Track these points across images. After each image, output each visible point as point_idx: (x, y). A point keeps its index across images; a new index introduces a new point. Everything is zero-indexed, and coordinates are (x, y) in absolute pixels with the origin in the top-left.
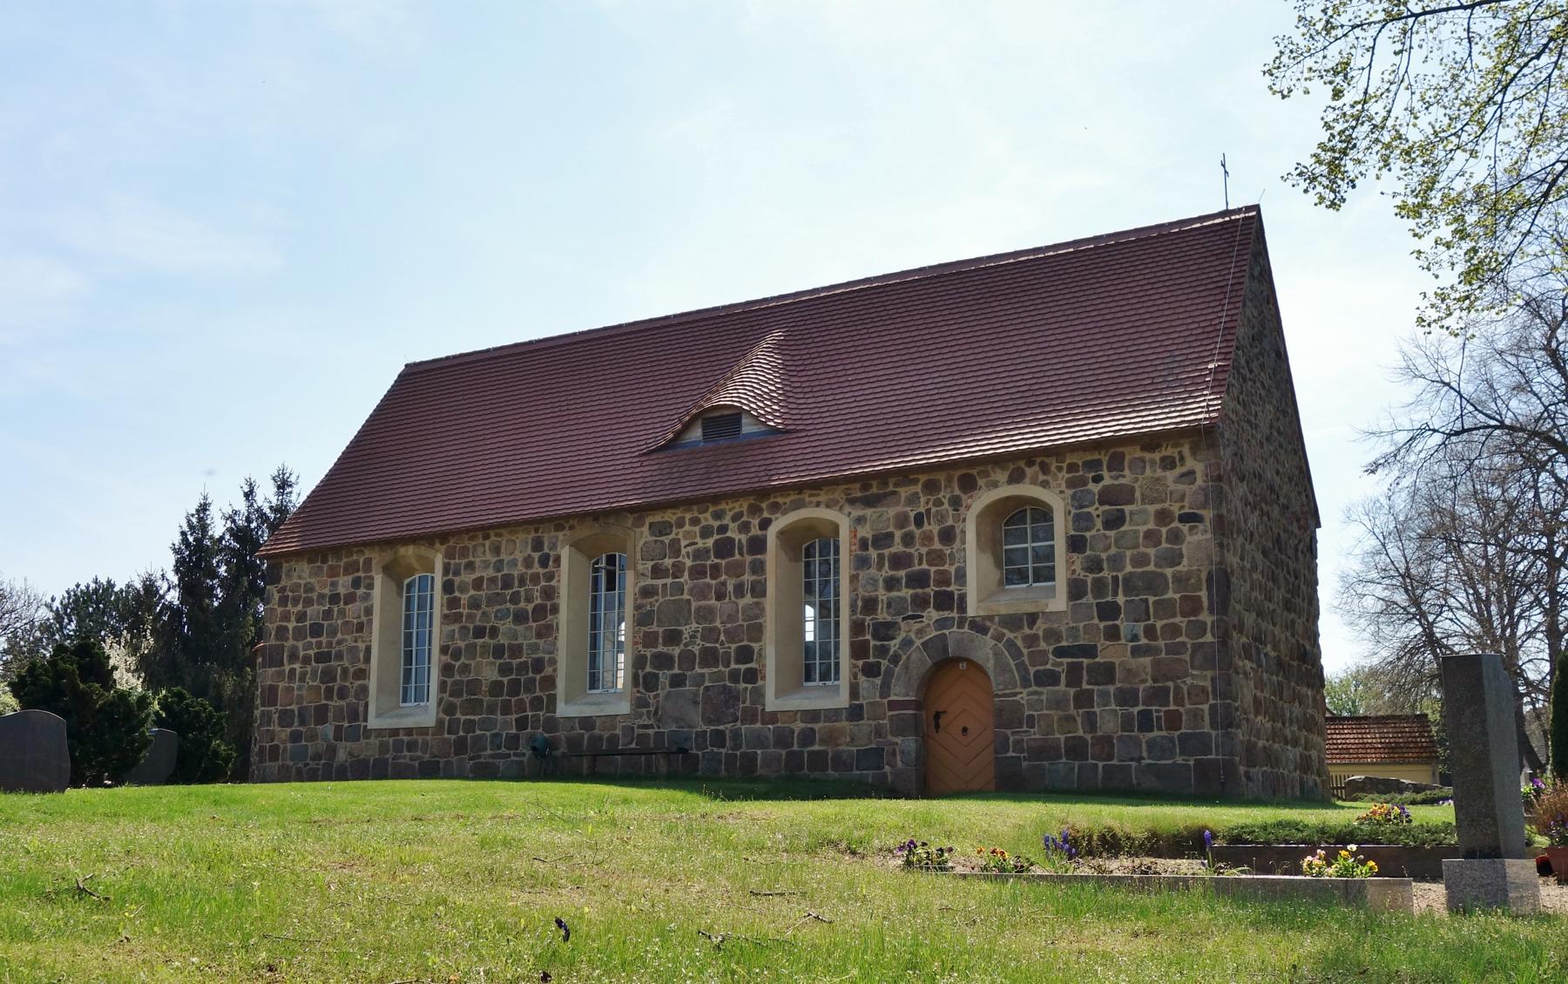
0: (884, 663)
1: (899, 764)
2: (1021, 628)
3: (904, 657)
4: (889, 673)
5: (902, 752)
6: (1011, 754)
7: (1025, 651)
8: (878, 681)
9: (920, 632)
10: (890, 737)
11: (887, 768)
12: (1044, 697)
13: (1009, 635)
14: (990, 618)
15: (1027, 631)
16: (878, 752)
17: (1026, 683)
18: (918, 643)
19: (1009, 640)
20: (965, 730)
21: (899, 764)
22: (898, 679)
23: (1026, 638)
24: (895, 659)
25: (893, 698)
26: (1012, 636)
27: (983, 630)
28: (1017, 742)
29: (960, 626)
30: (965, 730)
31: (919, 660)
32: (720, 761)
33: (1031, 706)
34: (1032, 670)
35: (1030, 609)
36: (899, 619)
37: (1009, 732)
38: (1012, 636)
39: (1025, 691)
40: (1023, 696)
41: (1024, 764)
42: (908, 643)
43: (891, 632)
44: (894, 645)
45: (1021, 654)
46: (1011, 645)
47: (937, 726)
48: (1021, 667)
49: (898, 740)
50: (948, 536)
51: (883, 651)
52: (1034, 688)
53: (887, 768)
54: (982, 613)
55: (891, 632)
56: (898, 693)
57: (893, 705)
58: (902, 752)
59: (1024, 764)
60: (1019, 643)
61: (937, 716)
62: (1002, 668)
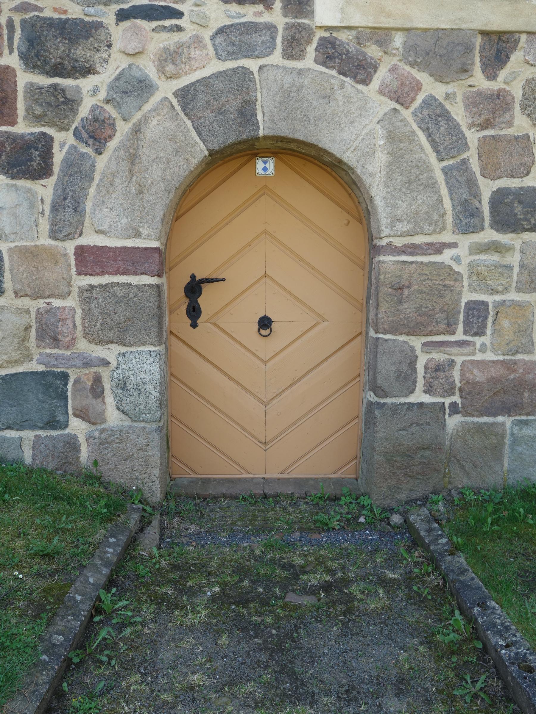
0: (63, 143)
1: (113, 417)
2: (465, 70)
3: (123, 129)
4: (78, 171)
5: (122, 385)
6: (418, 396)
7: (473, 137)
8: (45, 189)
9: (171, 58)
10: (83, 345)
11: (77, 427)
12: (514, 259)
13: (431, 87)
14: (381, 35)
15: (479, 80)
16: (52, 383)
17: (468, 218)
18: (166, 89)
19: (430, 102)
20: (265, 323)
21: (113, 417)
22: (108, 185)
23: (476, 101)
24: (96, 133)
25: (90, 239)
26: (439, 90)
27: (359, 69)
28: (437, 369)
29: (294, 45)
30: (265, 323)
31: (172, 144)
32: (485, 138)
33: (479, 278)
34: (487, 188)
35: (498, 21)
36: (107, 15)
37: (417, 342)
38: (439, 90)
39: (465, 242)
40: (460, 254)
41: (453, 422)
42: (133, 88)
43: (80, 52)
44: (91, 92)
45: (461, 144)
46: (435, 116)
47: (194, 313)
48: (461, 179)
49: (111, 353)
50: (101, 180)
51: (59, 105)
52: (490, 235)
53: (77, 427)
54: (358, 19)
55: (80, 52)
56: (106, 225)
57: (90, 259)
58: (122, 385)
59: (453, 422)
60: (459, 113)
61: (194, 288)
62: (409, 177)
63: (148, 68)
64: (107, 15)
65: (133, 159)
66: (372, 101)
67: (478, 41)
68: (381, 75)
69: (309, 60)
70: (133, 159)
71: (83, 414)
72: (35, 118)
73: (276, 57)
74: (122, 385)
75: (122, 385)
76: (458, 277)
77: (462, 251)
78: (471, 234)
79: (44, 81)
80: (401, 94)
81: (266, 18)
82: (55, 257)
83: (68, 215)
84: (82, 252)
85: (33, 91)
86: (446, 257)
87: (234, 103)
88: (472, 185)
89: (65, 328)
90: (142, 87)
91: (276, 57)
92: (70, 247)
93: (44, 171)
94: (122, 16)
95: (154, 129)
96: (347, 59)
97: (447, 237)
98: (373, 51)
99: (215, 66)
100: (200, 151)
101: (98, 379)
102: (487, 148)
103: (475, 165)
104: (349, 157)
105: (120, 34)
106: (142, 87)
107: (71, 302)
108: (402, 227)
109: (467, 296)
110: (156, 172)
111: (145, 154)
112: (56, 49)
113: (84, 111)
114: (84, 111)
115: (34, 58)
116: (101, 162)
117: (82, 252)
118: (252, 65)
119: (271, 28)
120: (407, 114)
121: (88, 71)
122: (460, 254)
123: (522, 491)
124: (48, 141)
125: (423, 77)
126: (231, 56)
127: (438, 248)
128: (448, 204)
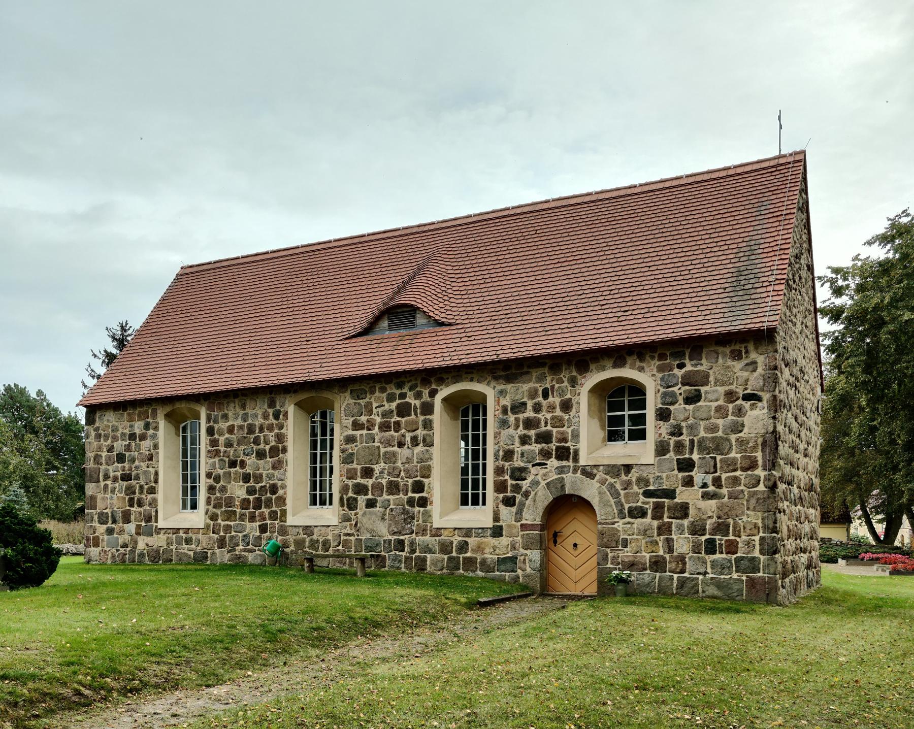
0: (519, 497)
1: (529, 570)
3: (533, 493)
4: (522, 505)
7: (622, 492)
10: (522, 551)
11: (519, 572)
15: (623, 477)
16: (513, 559)
17: (622, 515)
18: (543, 483)
20: (575, 545)
21: (529, 570)
24: (526, 495)
25: (524, 522)
26: (613, 480)
27: (591, 476)
29: (575, 471)
31: (543, 497)
34: (627, 506)
37: (608, 550)
40: (620, 525)
42: (536, 483)
43: (523, 475)
44: (525, 484)
46: (612, 487)
49: (528, 552)
51: (517, 488)
52: (628, 519)
53: (519, 572)
55: (523, 475)
60: (618, 486)
63: (539, 478)
64: (530, 466)
65: (534, 501)
66: (595, 484)
67: (622, 468)
68: (597, 477)
69: (579, 474)
70: (534, 501)
71: (520, 568)
72: (512, 491)
73: (570, 474)
74: (531, 560)
75: (531, 560)
76: (619, 531)
77: (620, 524)
78: (308, 452)
79: (514, 482)
80: (603, 482)
81: (568, 464)
82: (515, 527)
83: (519, 516)
84: (522, 525)
85: (512, 485)
86: (616, 526)
87: (559, 486)
88: (622, 505)
89: (517, 545)
90: (538, 483)
91: (570, 474)
92: (519, 524)
93: (514, 505)
94: (533, 466)
95: (540, 493)
96: (588, 473)
97: (616, 520)
98: (595, 471)
99: (556, 477)
100: (551, 499)
101: (524, 559)
102: (626, 495)
103: (623, 500)
104: (589, 499)
105: (533, 470)
106: (538, 483)
107: (519, 538)
108: (603, 517)
109: (622, 537)
110: (540, 504)
111: (537, 499)
112: (517, 474)
113: (523, 489)
114: (523, 489)
115: (512, 478)
116: (527, 502)
117: (522, 525)
118: (564, 476)
119: (569, 466)
120: (603, 487)
121: (524, 479)
122: (620, 525)
123: (286, 650)
124: (515, 497)
125: (608, 477)
126: (559, 474)
127: (614, 523)
128: (616, 511)
